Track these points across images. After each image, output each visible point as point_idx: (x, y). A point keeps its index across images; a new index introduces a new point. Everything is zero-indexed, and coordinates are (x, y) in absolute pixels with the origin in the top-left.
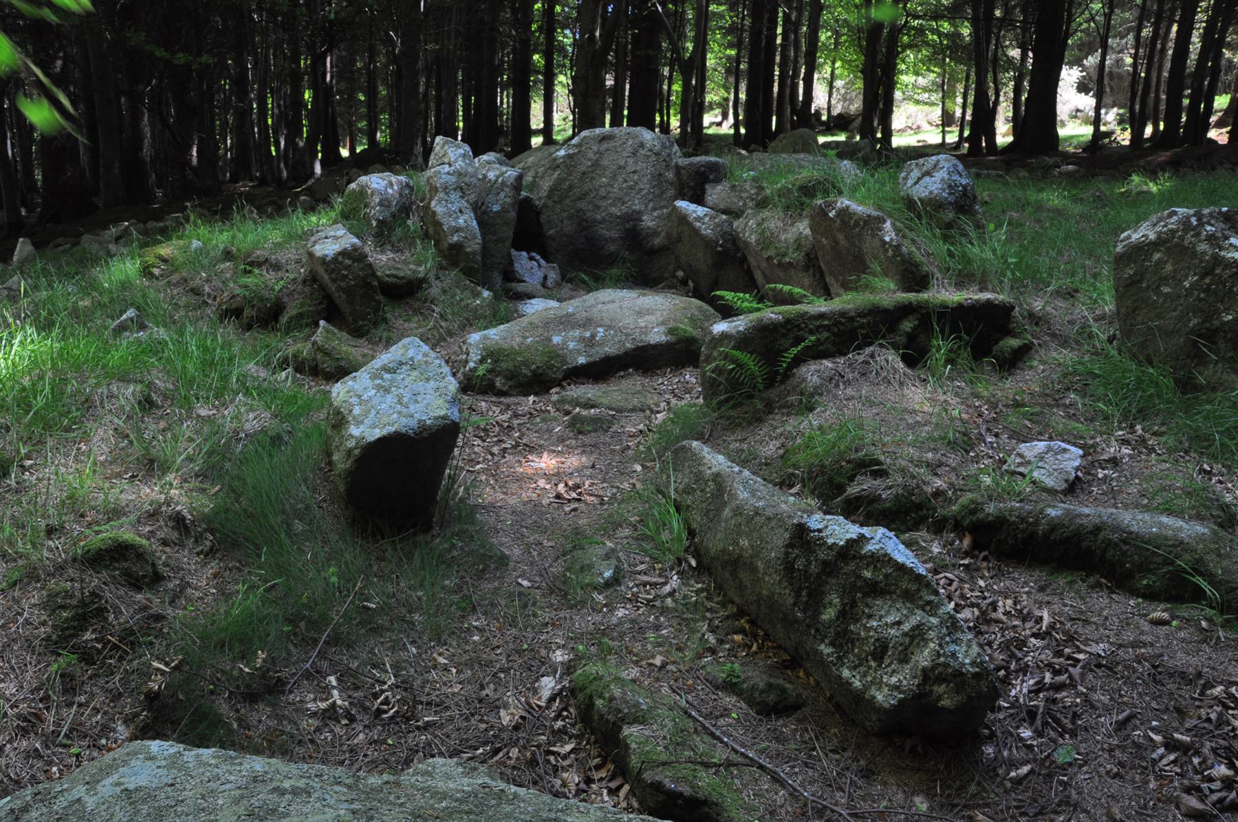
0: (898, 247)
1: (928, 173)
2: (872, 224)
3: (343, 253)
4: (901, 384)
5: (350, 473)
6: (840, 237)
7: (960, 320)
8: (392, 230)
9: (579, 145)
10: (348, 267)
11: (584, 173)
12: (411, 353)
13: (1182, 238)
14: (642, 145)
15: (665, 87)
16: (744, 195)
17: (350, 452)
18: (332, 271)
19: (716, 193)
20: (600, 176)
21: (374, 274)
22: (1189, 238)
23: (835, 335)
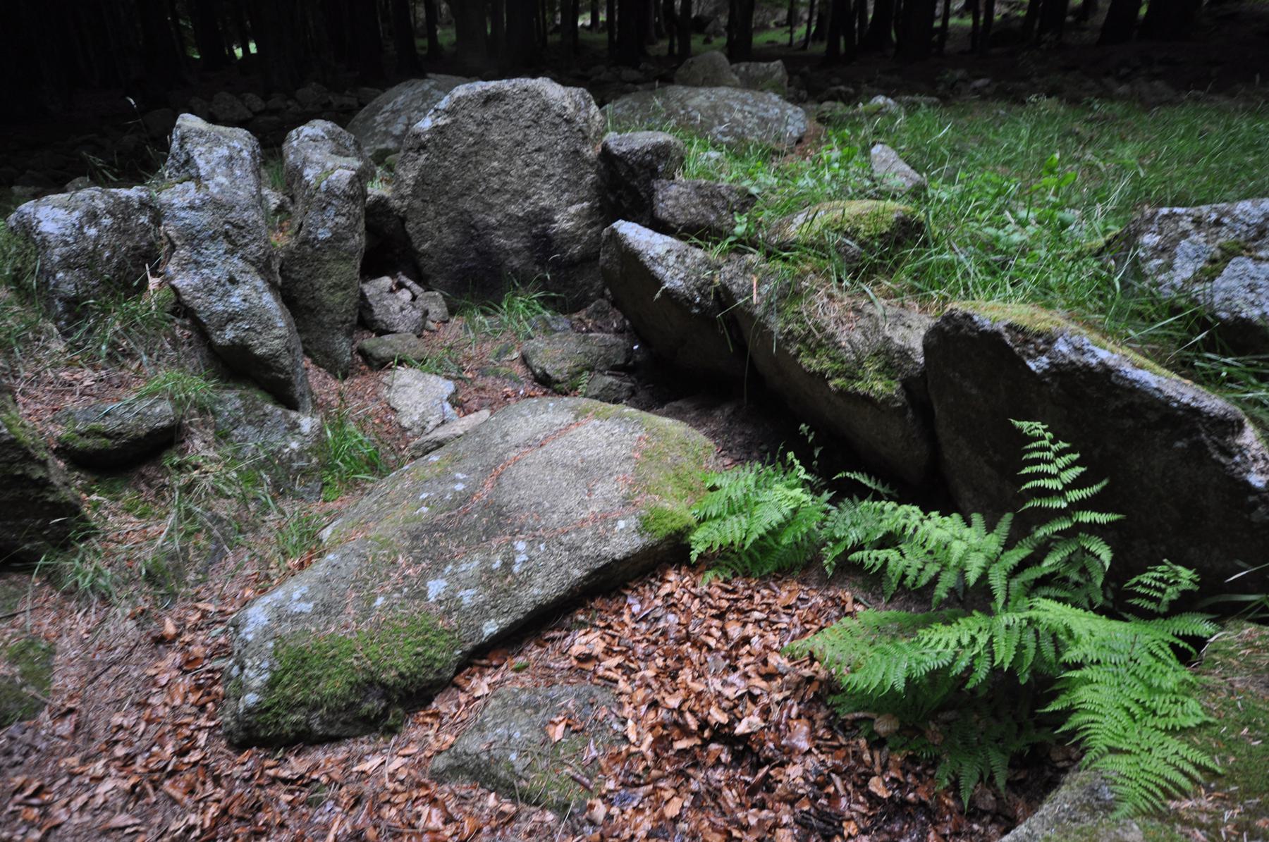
14: (546, 108)
20: (490, 159)
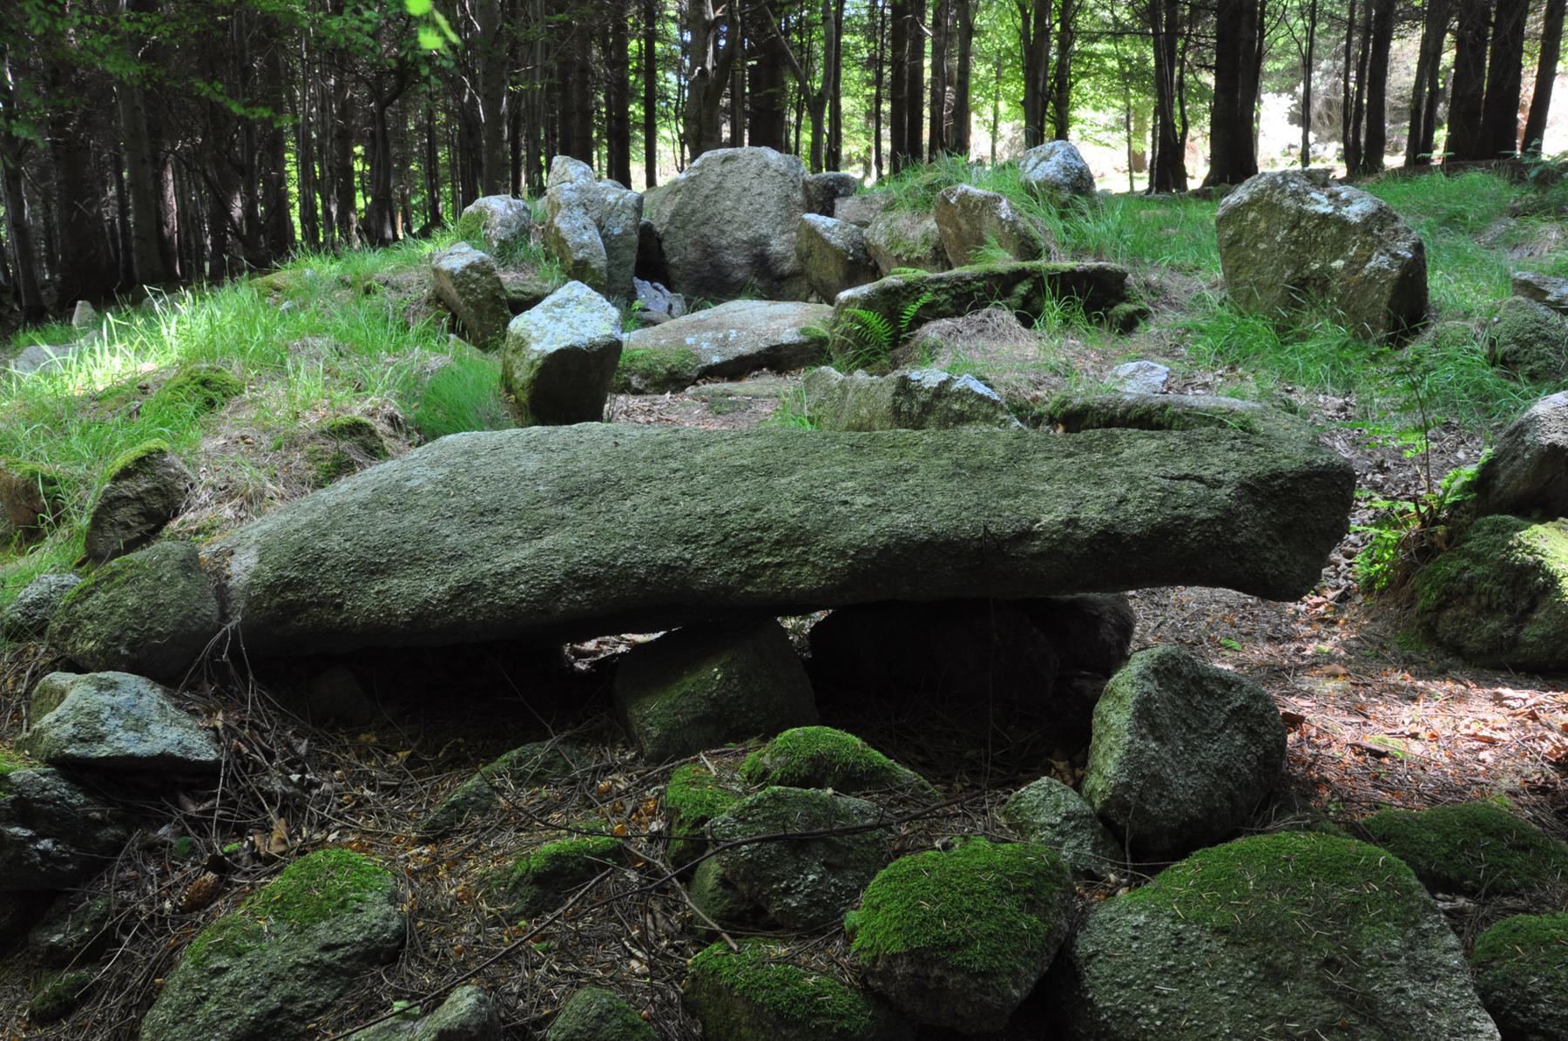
0: (1014, 222)
1: (1045, 159)
2: (989, 203)
3: (472, 267)
4: (1017, 339)
5: (533, 381)
6: (962, 222)
7: (1067, 283)
8: (513, 250)
9: (701, 167)
10: (476, 281)
12: (576, 292)
13: (1271, 196)
14: (767, 166)
15: (792, 138)
16: (875, 206)
17: (532, 364)
18: (461, 284)
19: (844, 206)
21: (501, 288)
22: (1276, 195)
23: (954, 297)
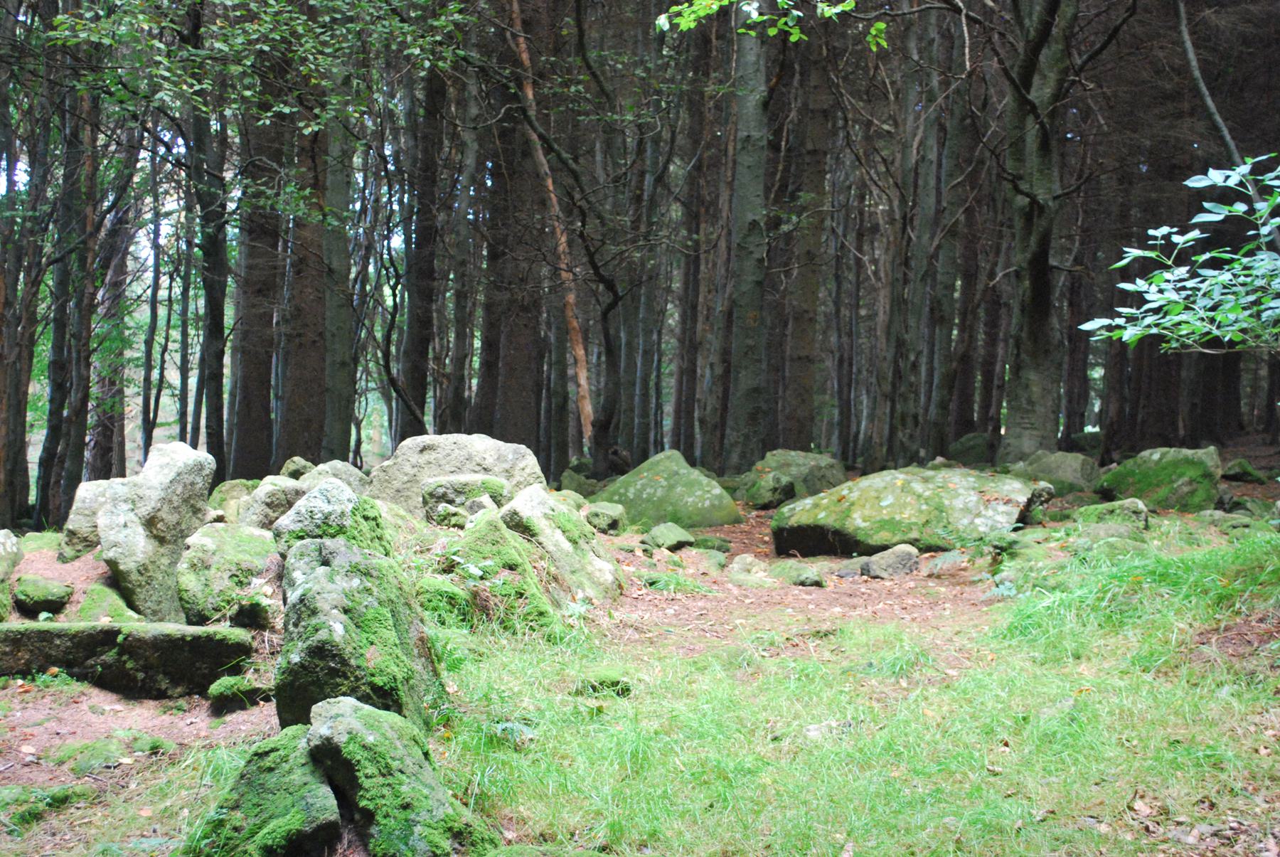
11: (398, 491)
